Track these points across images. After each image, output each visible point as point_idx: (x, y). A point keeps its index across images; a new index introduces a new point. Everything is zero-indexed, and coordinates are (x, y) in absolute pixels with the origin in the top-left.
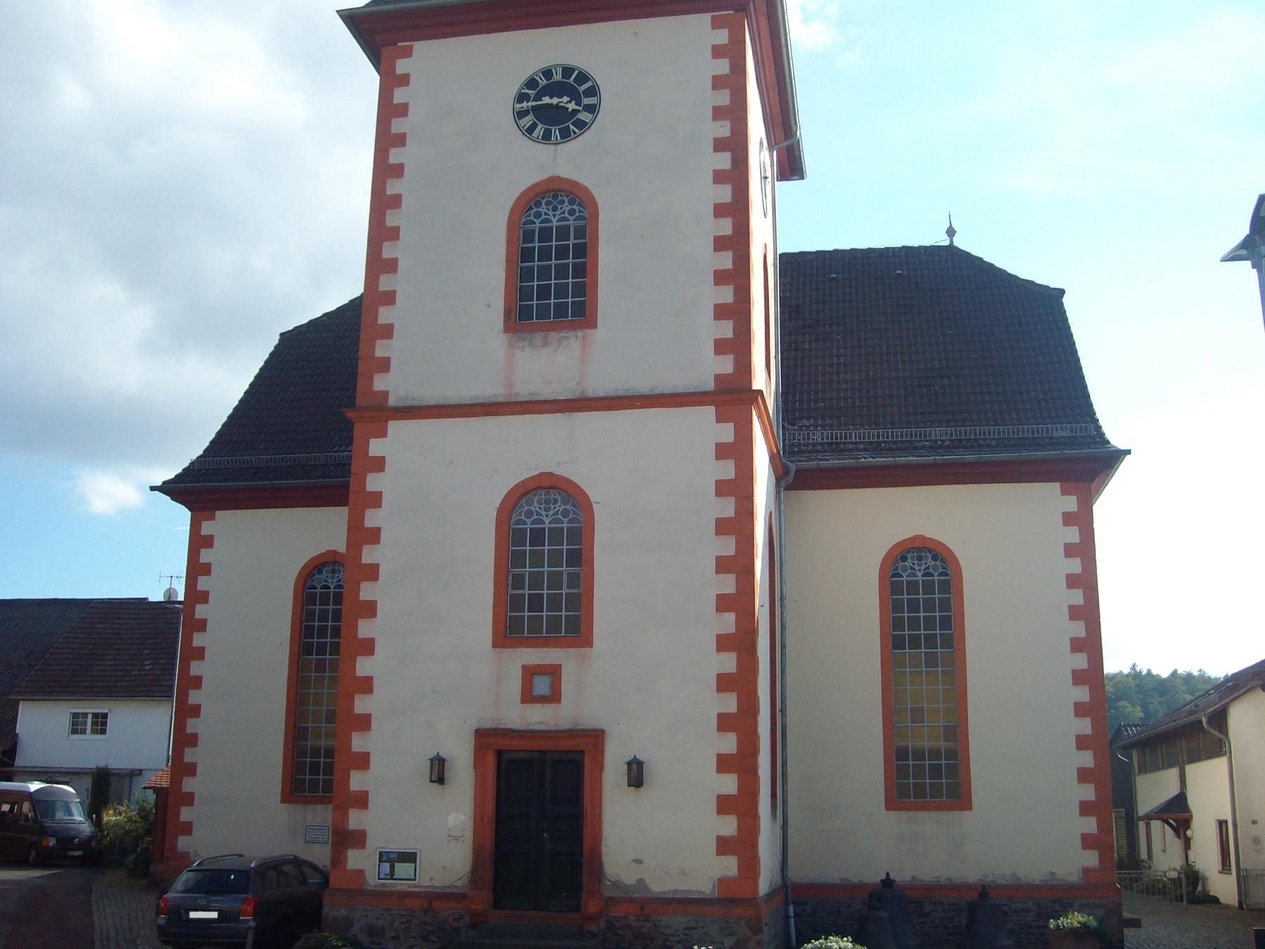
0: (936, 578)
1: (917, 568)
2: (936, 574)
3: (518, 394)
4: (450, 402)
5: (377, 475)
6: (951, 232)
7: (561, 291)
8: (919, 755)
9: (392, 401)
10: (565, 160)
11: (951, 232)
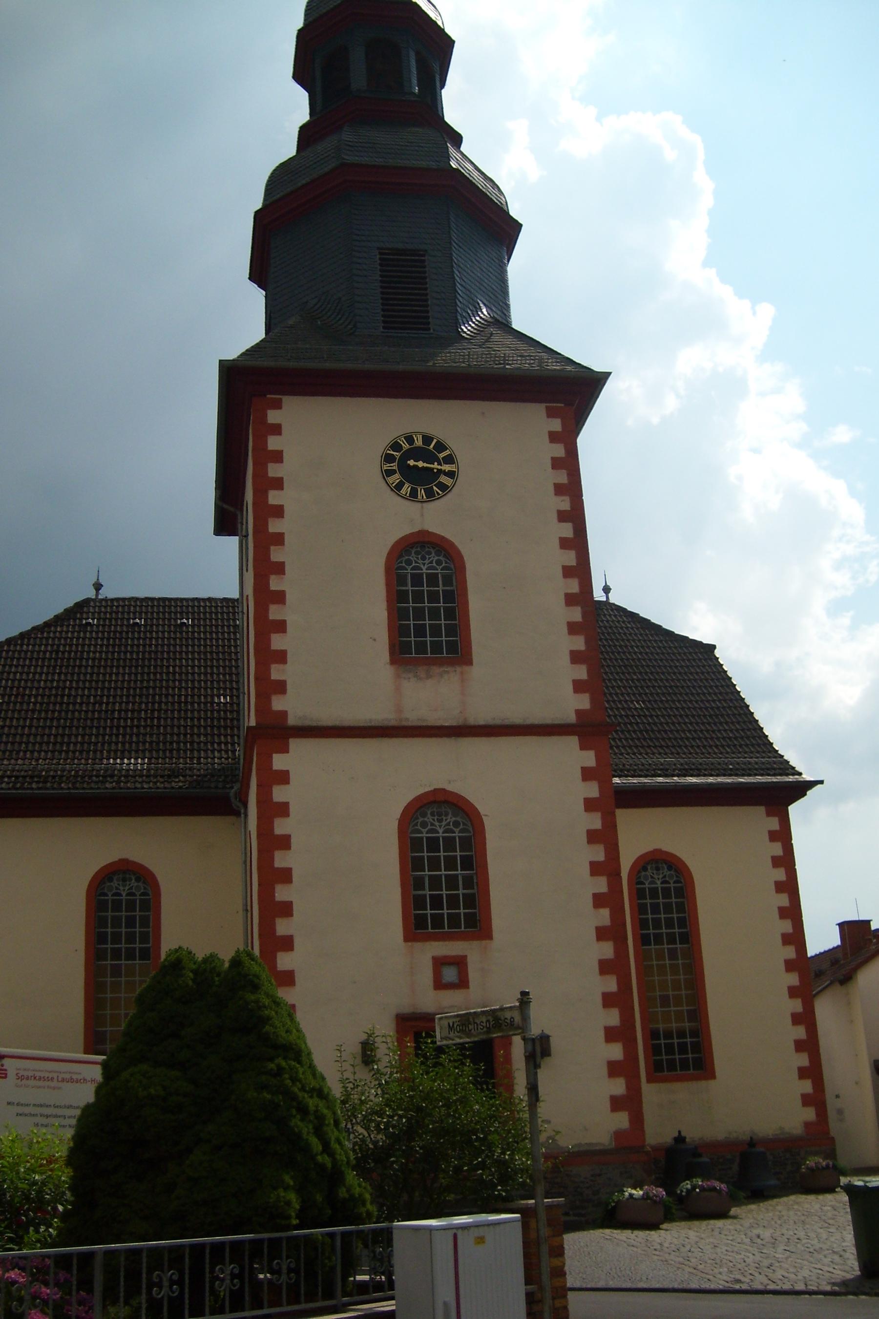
0: (672, 885)
1: (656, 876)
2: (672, 882)
3: (407, 719)
4: (346, 723)
5: (283, 787)
6: (98, 586)
7: (436, 631)
8: (668, 1035)
9: (291, 721)
10: (434, 517)
11: (98, 586)
